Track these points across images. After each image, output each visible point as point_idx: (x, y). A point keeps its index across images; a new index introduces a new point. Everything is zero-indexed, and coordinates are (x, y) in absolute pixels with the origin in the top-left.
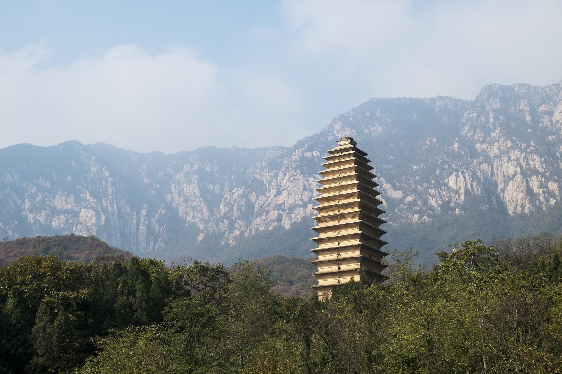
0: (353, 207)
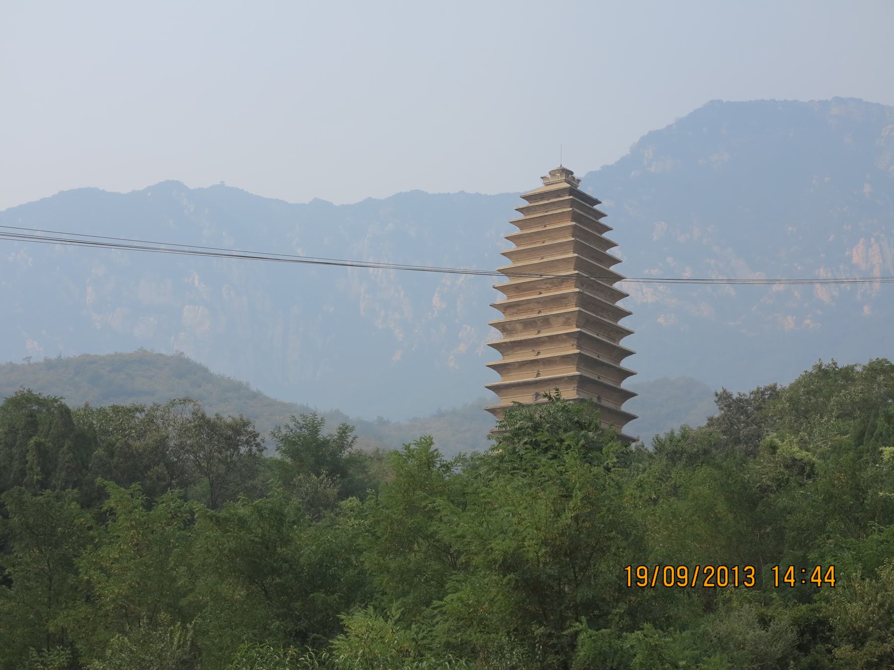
0: (566, 306)
